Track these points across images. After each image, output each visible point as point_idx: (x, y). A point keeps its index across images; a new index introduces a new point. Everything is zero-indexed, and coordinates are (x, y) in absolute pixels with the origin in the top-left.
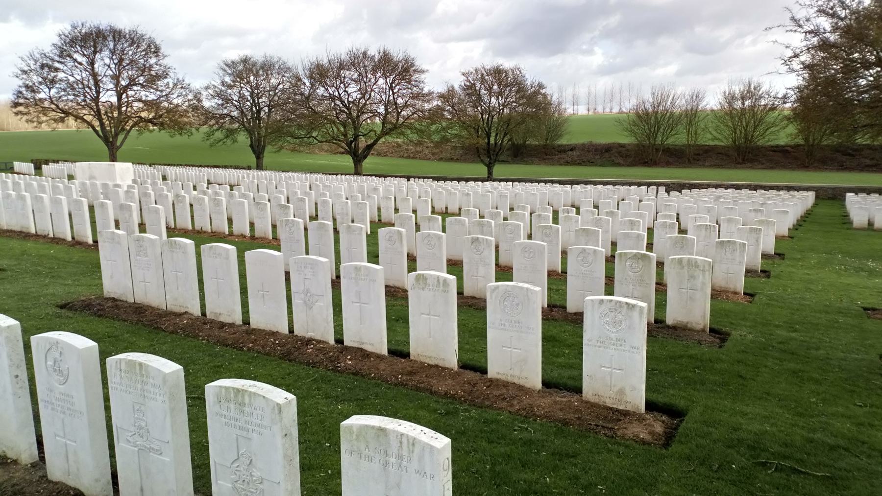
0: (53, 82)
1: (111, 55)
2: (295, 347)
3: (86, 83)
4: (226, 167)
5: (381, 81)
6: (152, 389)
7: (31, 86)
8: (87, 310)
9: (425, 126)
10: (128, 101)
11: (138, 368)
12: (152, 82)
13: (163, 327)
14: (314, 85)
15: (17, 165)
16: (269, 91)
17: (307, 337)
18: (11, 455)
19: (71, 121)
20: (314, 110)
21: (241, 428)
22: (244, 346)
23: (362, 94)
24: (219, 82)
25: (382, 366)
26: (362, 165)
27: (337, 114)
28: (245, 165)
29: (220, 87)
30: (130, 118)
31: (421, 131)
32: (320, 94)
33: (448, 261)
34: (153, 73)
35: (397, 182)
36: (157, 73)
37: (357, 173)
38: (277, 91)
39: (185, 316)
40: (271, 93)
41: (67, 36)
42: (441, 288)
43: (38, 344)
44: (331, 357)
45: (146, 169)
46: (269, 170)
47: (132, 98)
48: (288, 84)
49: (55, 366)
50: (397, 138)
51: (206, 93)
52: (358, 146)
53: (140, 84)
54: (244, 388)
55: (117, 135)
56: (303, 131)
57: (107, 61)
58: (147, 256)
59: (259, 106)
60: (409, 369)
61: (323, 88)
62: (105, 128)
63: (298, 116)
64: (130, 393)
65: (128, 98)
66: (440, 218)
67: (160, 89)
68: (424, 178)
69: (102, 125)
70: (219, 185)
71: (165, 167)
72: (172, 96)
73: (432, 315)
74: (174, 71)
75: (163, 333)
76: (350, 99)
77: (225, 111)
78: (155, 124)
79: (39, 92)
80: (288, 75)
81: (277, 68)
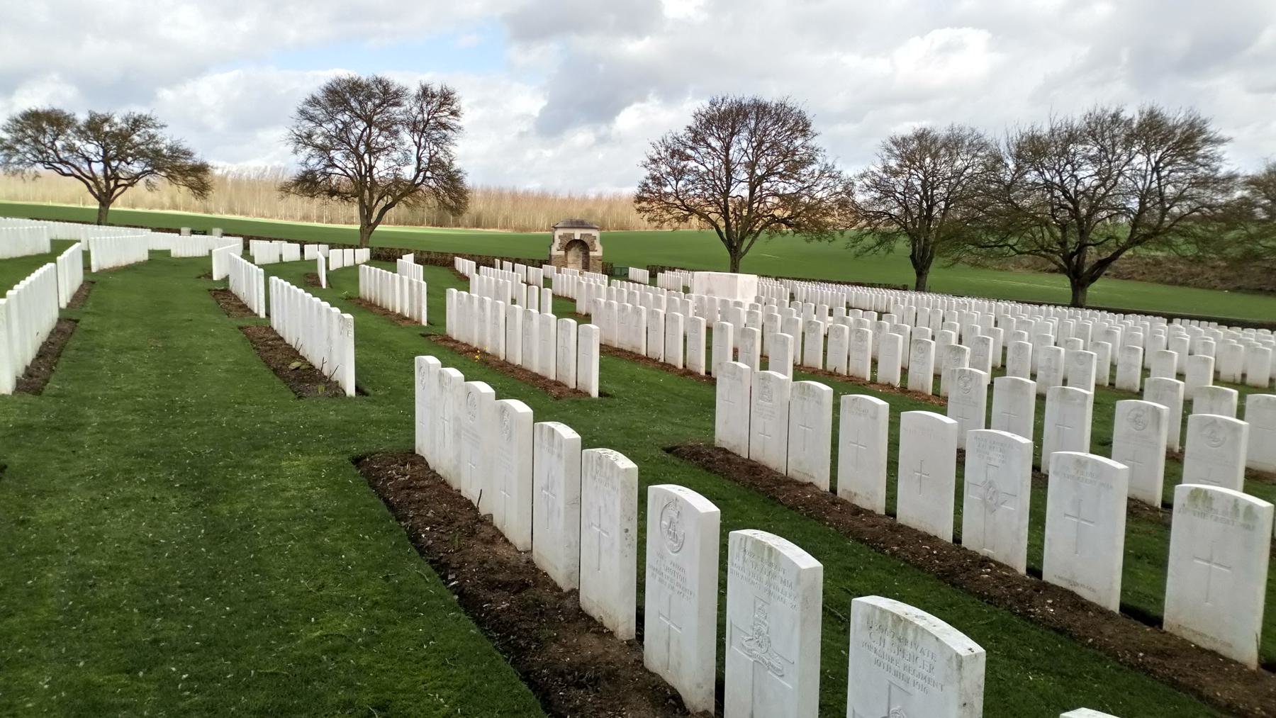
2: (962, 566)
4: (872, 285)
5: (1139, 160)
6: (781, 586)
9: (1213, 232)
10: (762, 195)
11: (766, 553)
12: (794, 168)
13: (781, 498)
14: (1022, 167)
15: (634, 272)
16: (949, 178)
17: (981, 554)
18: (608, 623)
19: (694, 220)
20: (1017, 205)
21: (896, 674)
22: (886, 548)
23: (1100, 179)
24: (881, 166)
25: (1108, 630)
26: (1086, 291)
27: (1053, 210)
28: (899, 284)
29: (881, 174)
30: (760, 216)
31: (1205, 241)
32: (1030, 181)
33: (1247, 469)
34: (797, 158)
35: (1148, 324)
36: (801, 158)
37: (1076, 303)
38: (962, 178)
39: (809, 488)
40: (952, 181)
41: (703, 116)
42: (1241, 520)
43: (655, 497)
44: (1019, 594)
45: (771, 284)
46: (933, 292)
47: (767, 192)
48: (981, 167)
50: (1157, 250)
51: (861, 183)
52: (1083, 262)
53: (779, 173)
54: (907, 617)
55: (742, 239)
56: (993, 236)
57: (744, 144)
59: (932, 200)
60: (1160, 646)
61: (1036, 173)
63: (989, 214)
64: (753, 583)
65: (762, 192)
66: (1235, 392)
67: (803, 179)
68: (1200, 319)
69: (728, 225)
70: (864, 310)
72: (816, 188)
73: (1216, 564)
74: (823, 153)
75: (780, 506)
76: (1080, 188)
77: (883, 208)
78: (789, 225)
79: (666, 185)
80: (982, 154)
81: (967, 144)
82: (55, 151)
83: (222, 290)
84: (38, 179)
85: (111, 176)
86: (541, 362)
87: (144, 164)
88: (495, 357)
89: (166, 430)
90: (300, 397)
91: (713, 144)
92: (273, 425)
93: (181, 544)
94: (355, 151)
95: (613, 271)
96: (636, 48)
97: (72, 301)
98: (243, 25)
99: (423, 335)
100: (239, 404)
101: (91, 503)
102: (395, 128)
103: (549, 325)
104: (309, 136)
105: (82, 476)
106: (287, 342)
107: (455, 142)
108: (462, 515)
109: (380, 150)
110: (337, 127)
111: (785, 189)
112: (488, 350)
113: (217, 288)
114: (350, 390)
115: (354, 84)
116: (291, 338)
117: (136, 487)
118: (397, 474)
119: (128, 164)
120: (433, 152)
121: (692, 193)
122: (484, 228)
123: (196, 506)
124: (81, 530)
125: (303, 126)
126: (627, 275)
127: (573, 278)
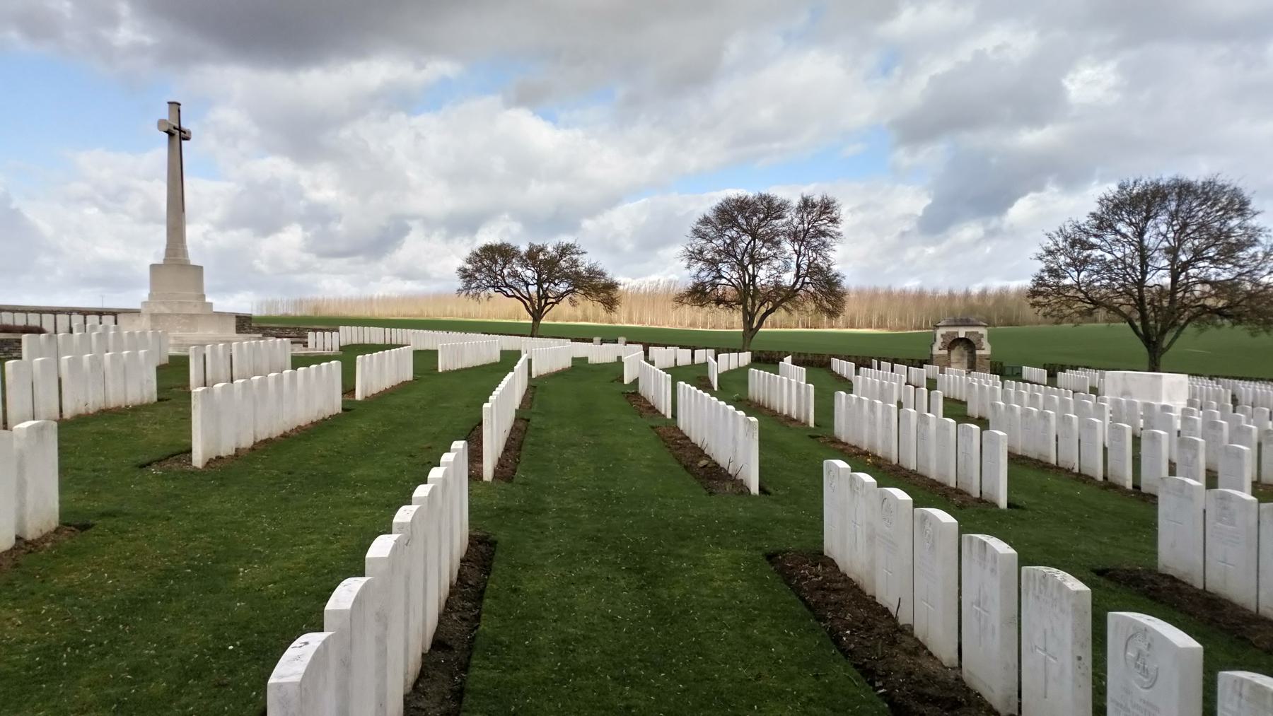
0: (1085, 262)
1: (1170, 220)
3: (1128, 261)
7: (1055, 270)
8: (1134, 586)
12: (1229, 252)
13: (1253, 639)
15: (1027, 371)
30: (1185, 306)
34: (1233, 240)
41: (1111, 201)
47: (1194, 279)
49: (1138, 660)
55: (1164, 332)
57: (1163, 228)
58: (1233, 524)
62: (1148, 322)
67: (1242, 263)
69: (1144, 318)
71: (1236, 381)
74: (1268, 233)
79: (1065, 277)
82: (503, 277)
83: (633, 393)
84: (917, 385)
85: (543, 296)
86: (938, 467)
87: (567, 285)
88: (887, 461)
89: (608, 518)
90: (711, 493)
91: (1124, 230)
92: (692, 519)
93: (634, 621)
94: (740, 263)
95: (1005, 370)
96: (1031, 139)
97: (522, 403)
98: (654, 160)
99: (811, 437)
100: (661, 497)
101: (562, 578)
102: (777, 239)
103: (948, 430)
104: (701, 252)
105: (552, 554)
106: (693, 441)
107: (833, 247)
108: (881, 622)
109: (762, 260)
110: (725, 242)
111: (1219, 275)
112: (879, 454)
113: (628, 391)
114: (755, 489)
115: (742, 202)
116: (696, 438)
117: (593, 567)
118: (810, 575)
119: (556, 285)
120: (811, 258)
121: (1097, 284)
122: (858, 328)
123: (641, 588)
124: (558, 601)
125: (696, 243)
126: (1020, 374)
127: (961, 379)
